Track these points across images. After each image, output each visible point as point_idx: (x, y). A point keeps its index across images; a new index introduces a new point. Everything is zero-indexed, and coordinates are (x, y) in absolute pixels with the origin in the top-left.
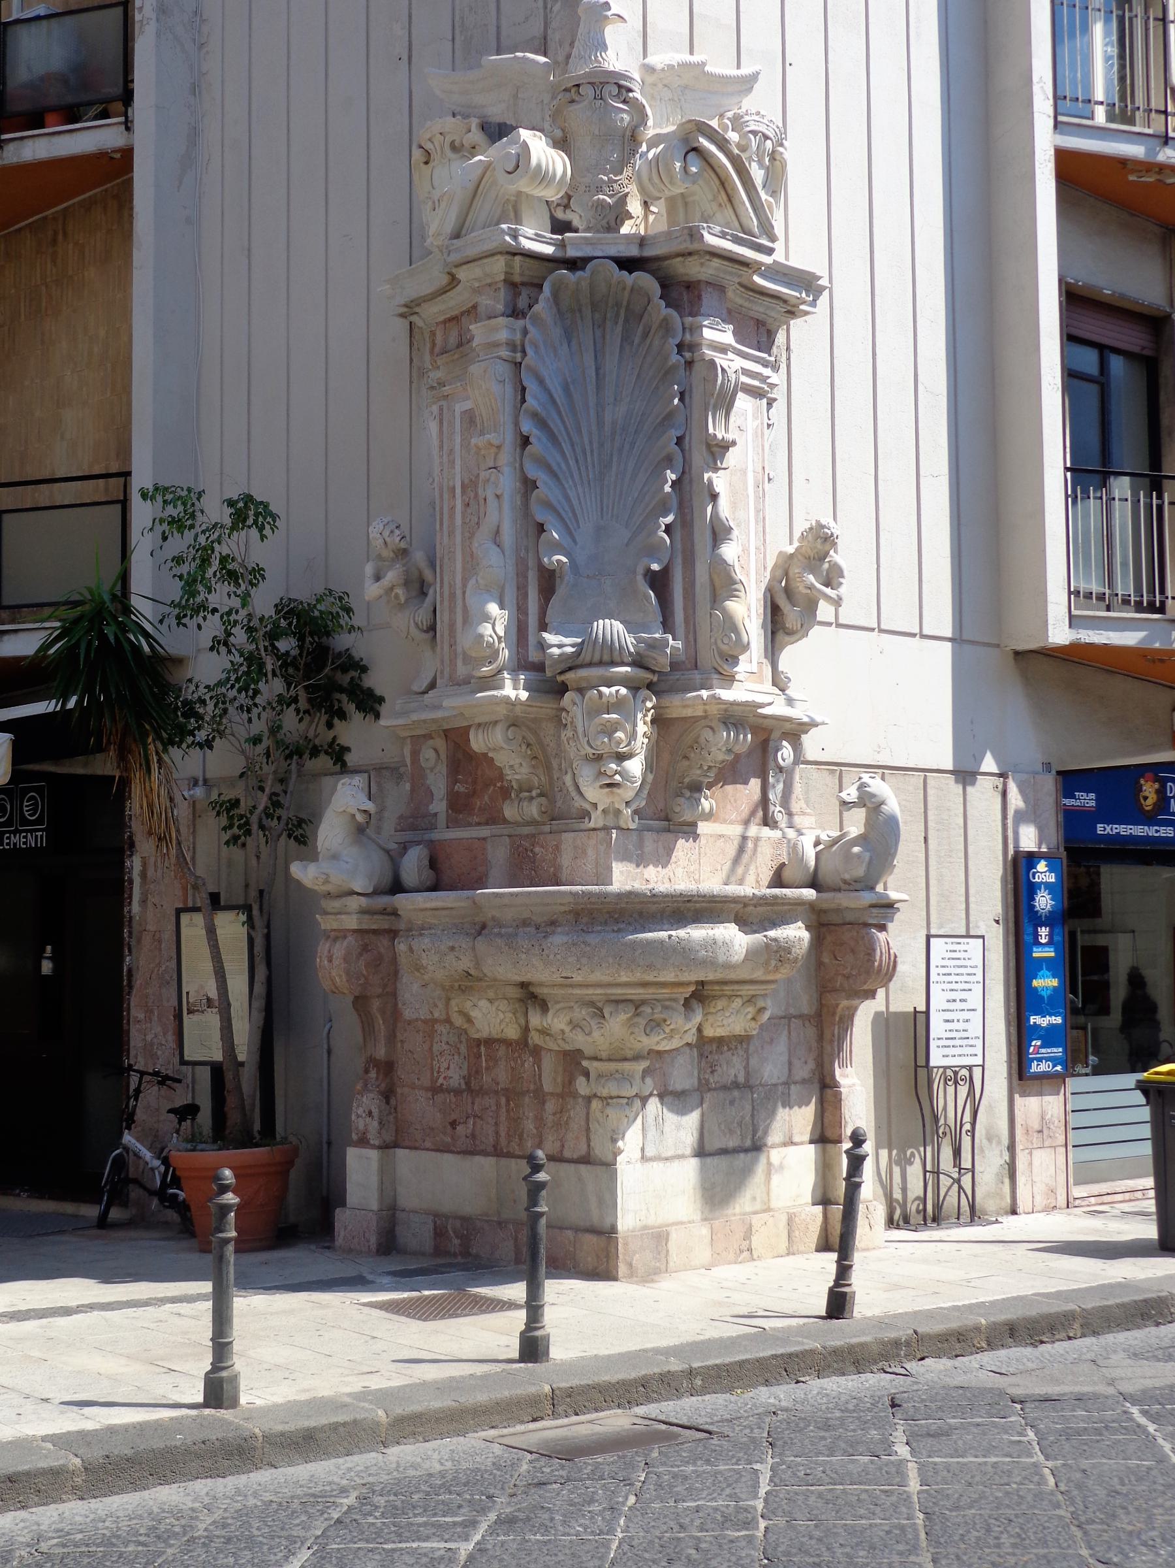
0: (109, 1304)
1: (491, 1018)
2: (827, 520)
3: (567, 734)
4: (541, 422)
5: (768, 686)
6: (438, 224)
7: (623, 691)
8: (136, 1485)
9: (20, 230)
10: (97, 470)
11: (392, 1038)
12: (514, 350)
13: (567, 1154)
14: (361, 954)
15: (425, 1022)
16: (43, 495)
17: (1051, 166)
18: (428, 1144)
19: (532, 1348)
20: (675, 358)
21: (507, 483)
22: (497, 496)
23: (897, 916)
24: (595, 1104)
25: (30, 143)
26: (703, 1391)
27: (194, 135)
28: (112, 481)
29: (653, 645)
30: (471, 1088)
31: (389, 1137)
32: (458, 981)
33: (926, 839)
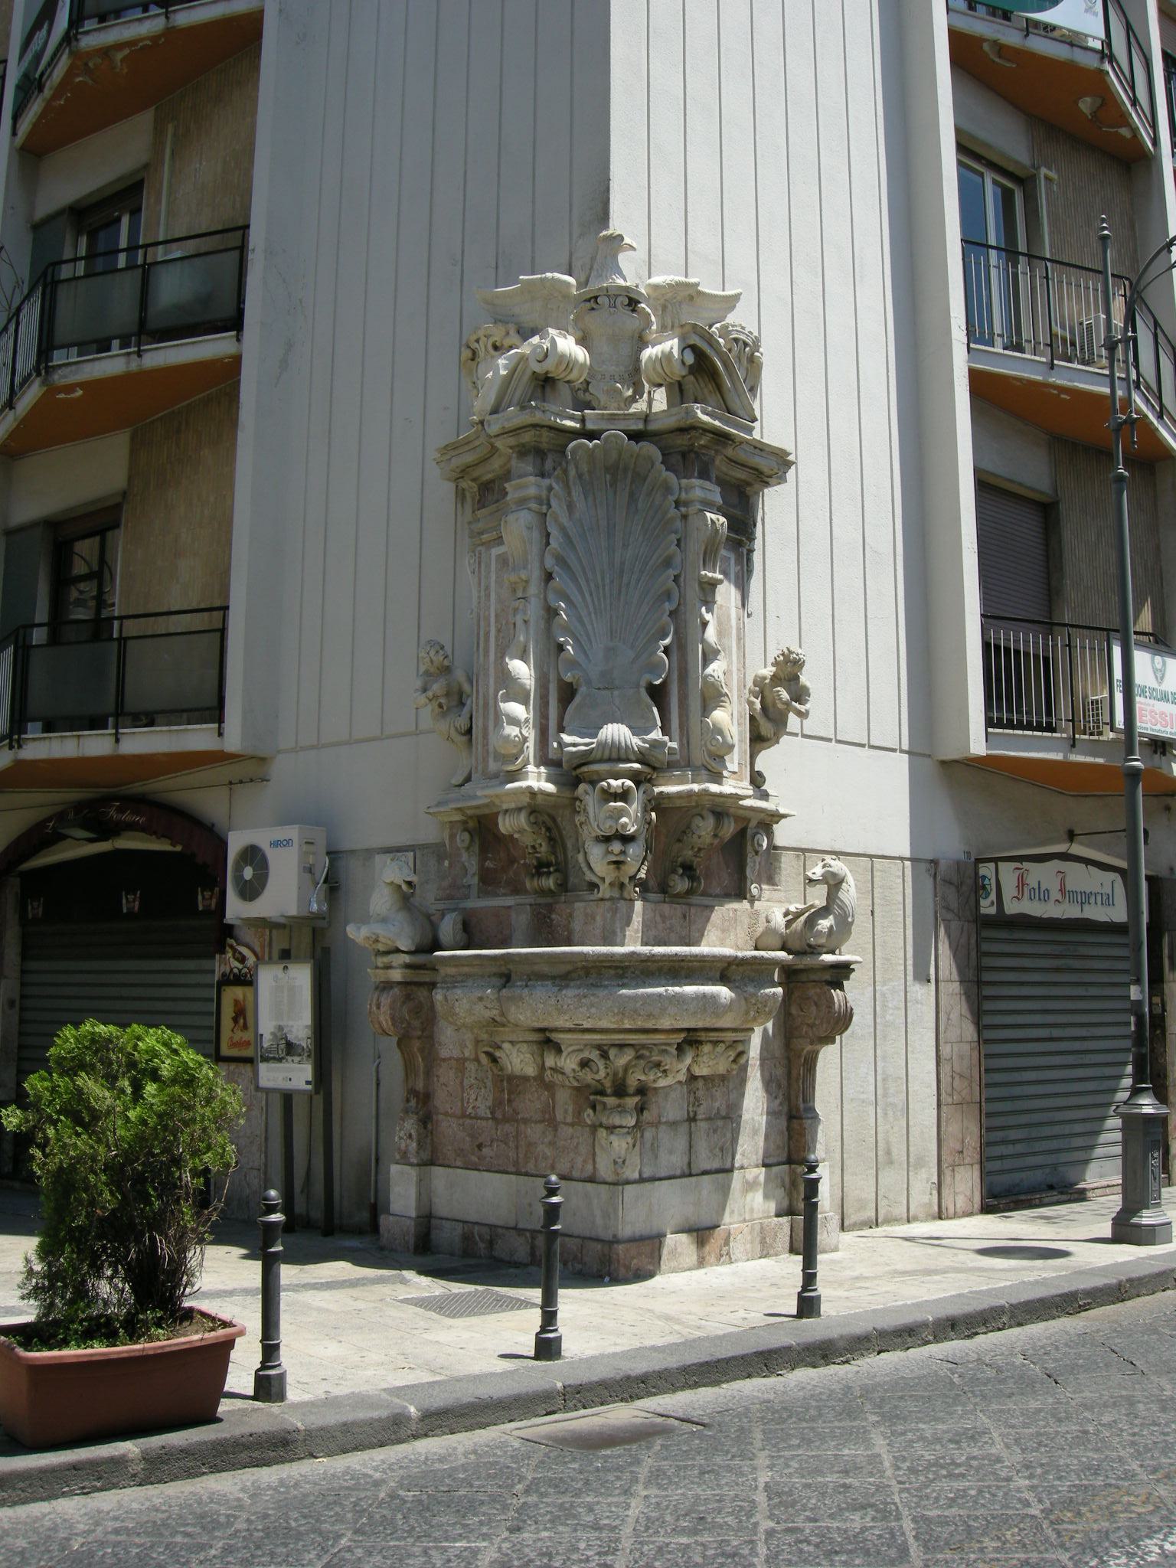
2: (795, 648)
3: (578, 819)
4: (561, 561)
5: (746, 783)
7: (629, 783)
8: (191, 1474)
9: (152, 422)
10: (202, 606)
12: (541, 504)
13: (576, 1174)
14: (404, 1003)
15: (457, 1060)
17: (966, 381)
18: (459, 1163)
19: (547, 1348)
20: (673, 512)
21: (533, 610)
22: (525, 622)
23: (852, 976)
24: (602, 1133)
25: (161, 352)
28: (215, 613)
29: (656, 745)
31: (425, 1155)
33: (872, 912)
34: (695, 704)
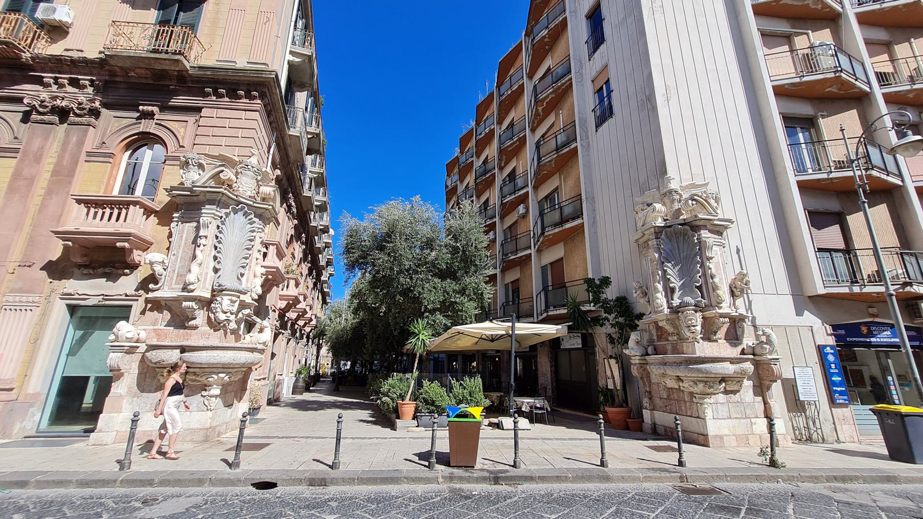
0: (387, 479)
1: (671, 383)
6: (640, 224)
11: (650, 386)
16: (575, 283)
26: (730, 481)
27: (594, 218)
29: (699, 301)
30: (669, 398)
32: (663, 376)
34: (711, 290)
